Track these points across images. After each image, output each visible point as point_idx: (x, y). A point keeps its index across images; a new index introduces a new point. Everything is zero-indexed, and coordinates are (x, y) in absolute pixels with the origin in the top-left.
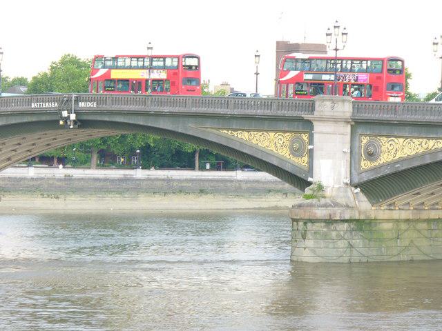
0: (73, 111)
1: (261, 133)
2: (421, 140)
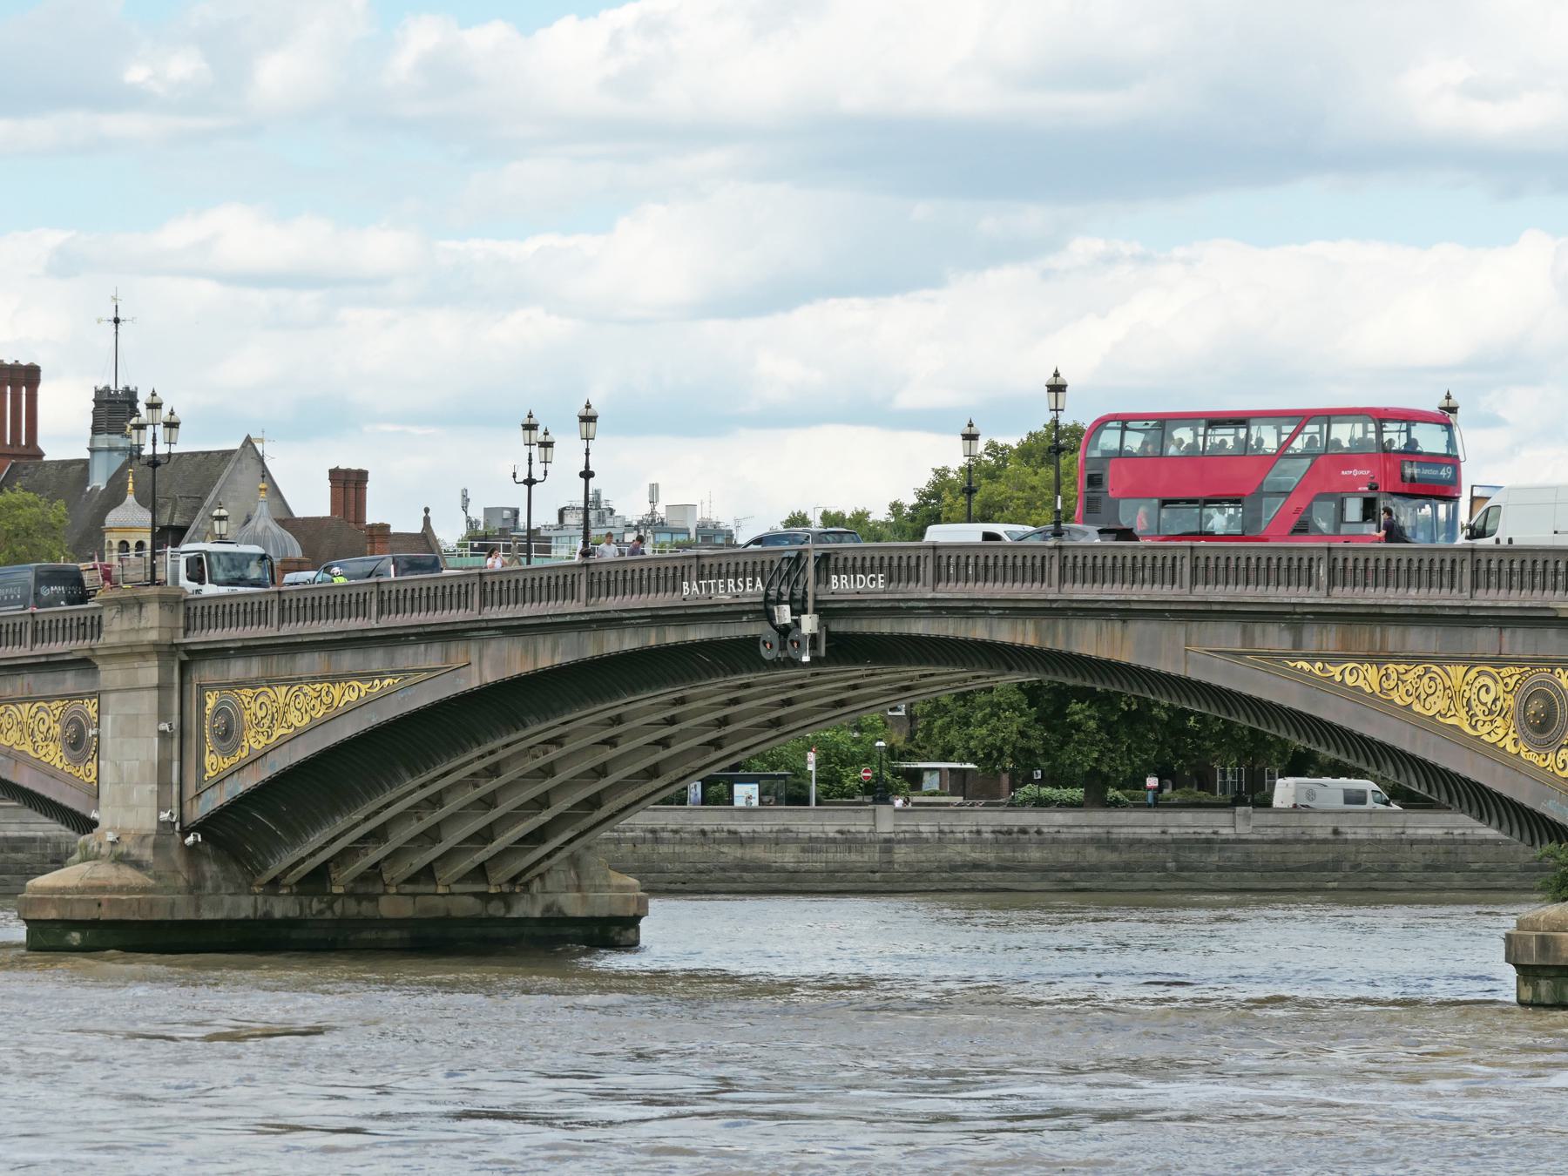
0: (810, 605)
1: (1420, 669)
2: (318, 686)
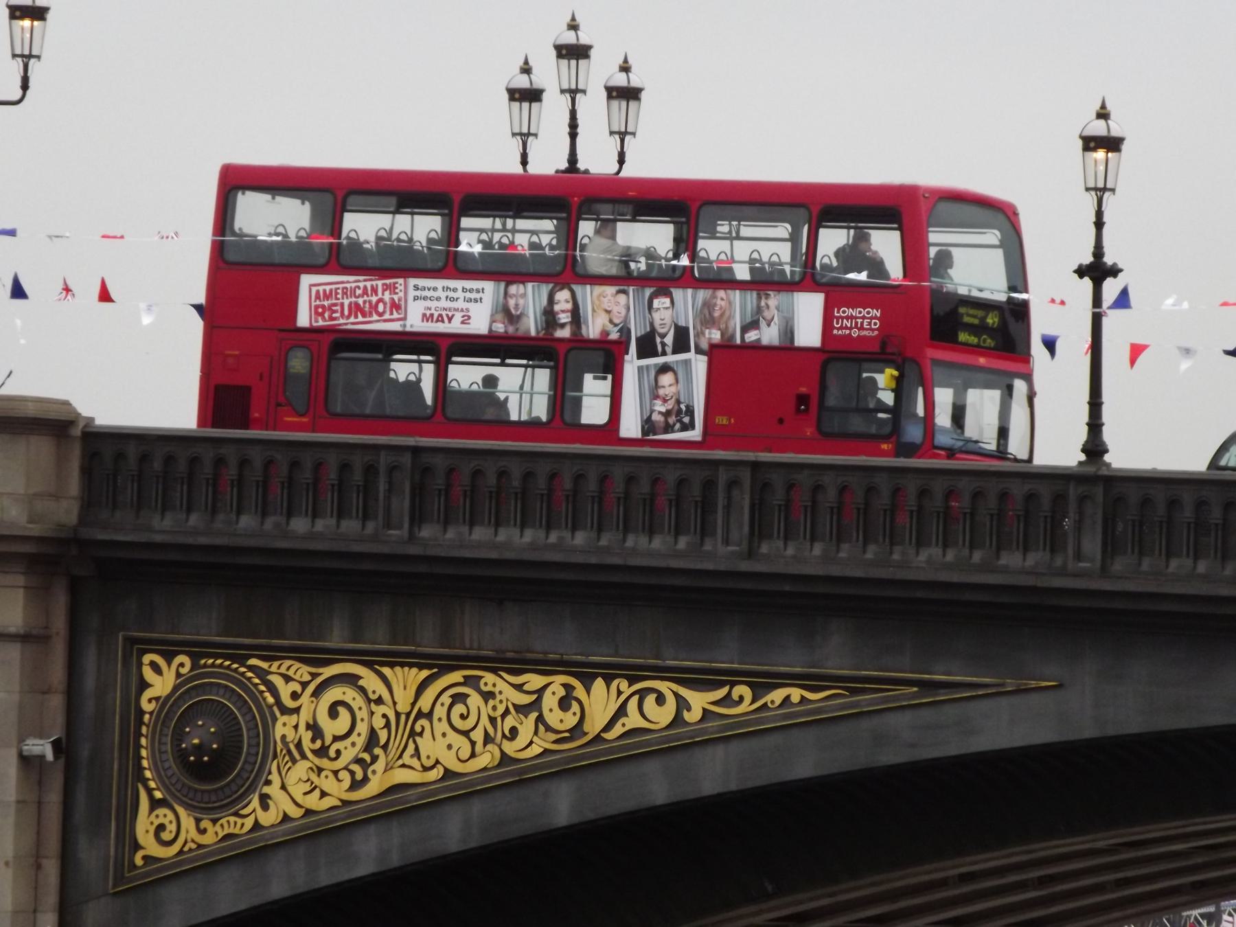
2: (534, 681)
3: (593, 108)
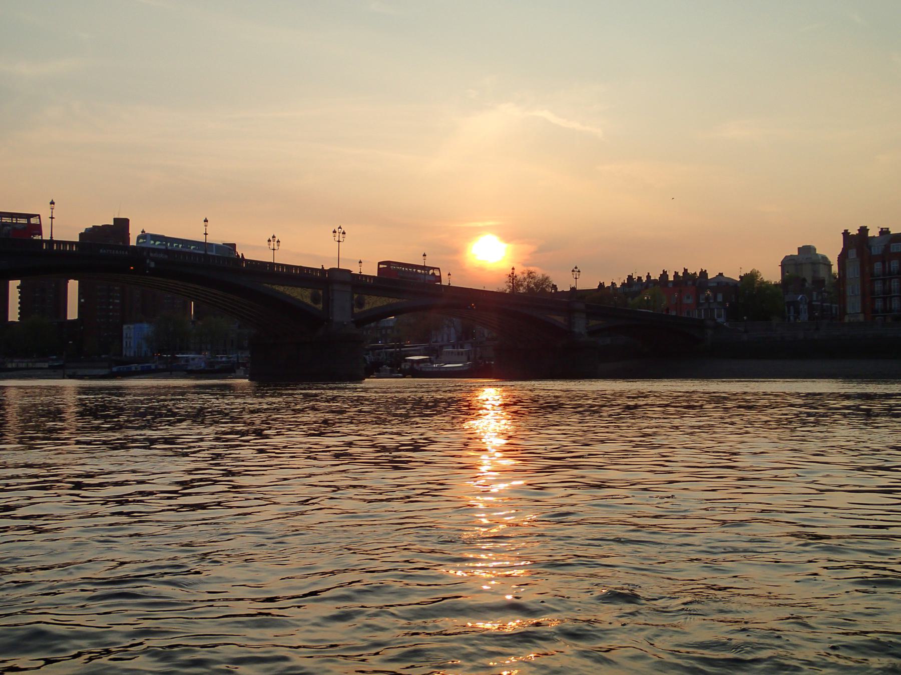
3: (276, 243)
